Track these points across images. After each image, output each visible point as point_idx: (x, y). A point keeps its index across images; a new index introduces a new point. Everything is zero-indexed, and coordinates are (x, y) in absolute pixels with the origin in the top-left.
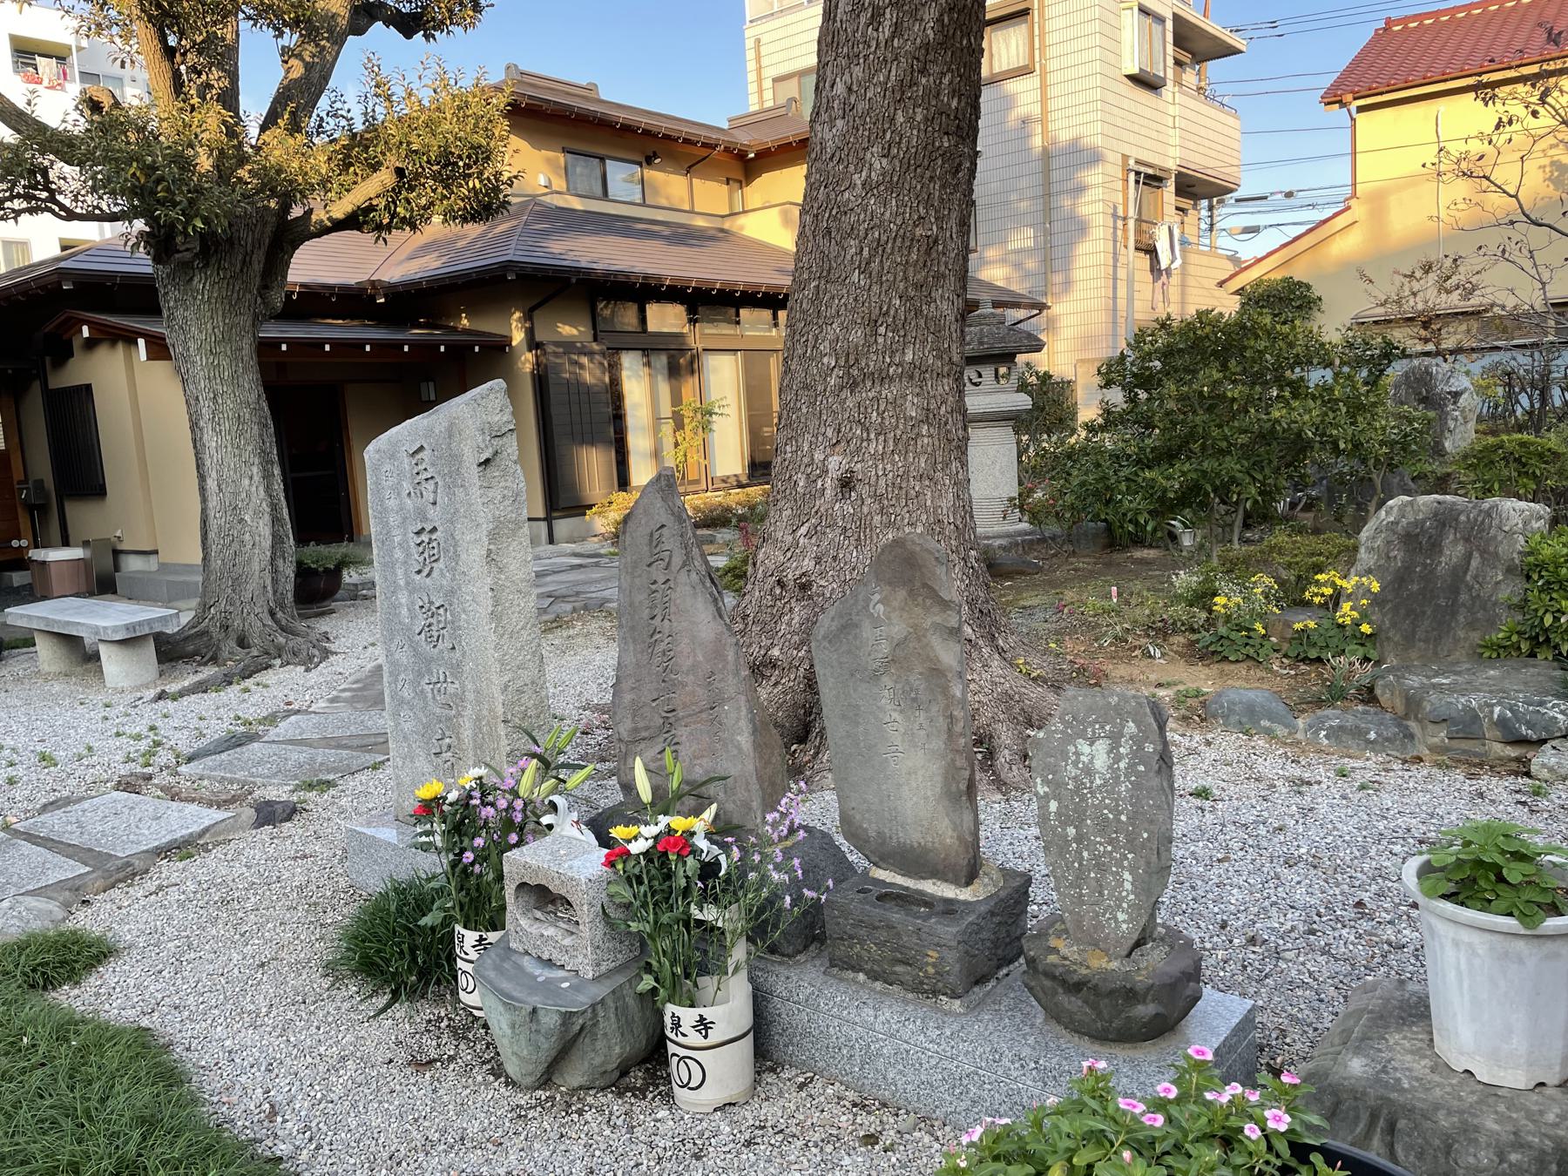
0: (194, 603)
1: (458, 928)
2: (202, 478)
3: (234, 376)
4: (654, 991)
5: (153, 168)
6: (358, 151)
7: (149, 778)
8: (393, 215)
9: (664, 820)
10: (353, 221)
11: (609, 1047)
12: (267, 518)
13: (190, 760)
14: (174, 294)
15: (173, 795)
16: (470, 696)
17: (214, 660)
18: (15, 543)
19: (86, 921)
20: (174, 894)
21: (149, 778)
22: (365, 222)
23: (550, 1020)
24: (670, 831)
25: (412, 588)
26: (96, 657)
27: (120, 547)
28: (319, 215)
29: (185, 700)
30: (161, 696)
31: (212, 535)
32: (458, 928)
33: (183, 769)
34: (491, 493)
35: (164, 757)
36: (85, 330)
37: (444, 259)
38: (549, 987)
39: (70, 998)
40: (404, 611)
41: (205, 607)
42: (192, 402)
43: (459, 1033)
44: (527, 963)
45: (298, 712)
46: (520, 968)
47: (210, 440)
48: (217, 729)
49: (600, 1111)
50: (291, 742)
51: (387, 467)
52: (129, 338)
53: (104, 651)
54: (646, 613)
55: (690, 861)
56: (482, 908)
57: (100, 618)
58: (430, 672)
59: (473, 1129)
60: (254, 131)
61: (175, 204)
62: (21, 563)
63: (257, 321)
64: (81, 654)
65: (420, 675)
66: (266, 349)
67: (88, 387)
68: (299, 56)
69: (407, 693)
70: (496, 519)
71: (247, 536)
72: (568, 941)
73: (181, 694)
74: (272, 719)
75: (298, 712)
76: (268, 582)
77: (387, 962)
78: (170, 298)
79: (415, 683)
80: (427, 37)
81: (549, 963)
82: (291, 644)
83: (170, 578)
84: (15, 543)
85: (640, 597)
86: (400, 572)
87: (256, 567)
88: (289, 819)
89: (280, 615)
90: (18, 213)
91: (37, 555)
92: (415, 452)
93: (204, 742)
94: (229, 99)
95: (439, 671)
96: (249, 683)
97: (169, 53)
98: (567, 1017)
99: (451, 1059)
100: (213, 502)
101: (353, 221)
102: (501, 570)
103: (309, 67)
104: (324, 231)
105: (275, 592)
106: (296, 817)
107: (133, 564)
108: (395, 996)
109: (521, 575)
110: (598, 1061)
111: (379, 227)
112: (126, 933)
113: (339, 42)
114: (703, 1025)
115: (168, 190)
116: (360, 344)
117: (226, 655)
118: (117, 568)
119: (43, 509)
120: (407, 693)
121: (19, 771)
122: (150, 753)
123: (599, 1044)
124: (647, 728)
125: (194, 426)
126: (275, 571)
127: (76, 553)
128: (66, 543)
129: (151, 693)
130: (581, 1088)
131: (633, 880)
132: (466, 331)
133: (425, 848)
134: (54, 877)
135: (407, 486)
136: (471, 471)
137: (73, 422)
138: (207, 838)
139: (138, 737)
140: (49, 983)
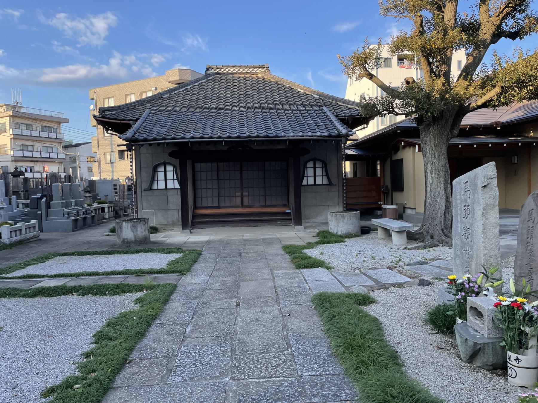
0: (420, 225)
1: (457, 318)
2: (426, 187)
3: (439, 156)
4: (504, 347)
5: (419, 100)
6: (487, 82)
7: (396, 267)
8: (500, 101)
9: (515, 298)
10: (485, 105)
11: (488, 357)
12: (444, 200)
13: (407, 265)
14: (424, 133)
15: (401, 273)
16: (475, 256)
17: (423, 241)
18: (379, 203)
19: (371, 294)
20: (393, 294)
21: (396, 267)
22: (489, 105)
23: (470, 343)
24: (516, 301)
25: (462, 222)
26: (390, 236)
27: (407, 206)
28: (473, 105)
29: (411, 251)
30: (405, 248)
31: (427, 204)
32: (457, 318)
33: (405, 267)
34: (485, 196)
35: (401, 263)
36: (403, 143)
37: (525, 112)
38: (474, 336)
39: (364, 308)
40: (459, 229)
41: (423, 225)
42: (426, 164)
43: (452, 345)
44: (470, 329)
45: (441, 259)
46: (467, 330)
47: (430, 176)
48: (417, 259)
49: (484, 374)
50: (436, 267)
51: (458, 187)
52: (414, 145)
53: (394, 234)
54: (526, 236)
55: (521, 311)
56: (463, 314)
57: (394, 224)
58: (465, 247)
59: (446, 364)
60: (455, 79)
61: (424, 109)
62: (380, 208)
63: (448, 139)
64: (387, 232)
65: (462, 248)
66: (451, 149)
67: (402, 159)
68: (472, 55)
69: (458, 253)
70: (486, 204)
71: (437, 206)
72: (482, 326)
73: (411, 249)
74: (433, 260)
75: (441, 259)
76: (442, 220)
77: (438, 322)
78: (423, 134)
79: (461, 250)
80: (521, 38)
81: (476, 331)
82: (446, 240)
83: (418, 217)
84: (379, 203)
85: (525, 231)
86: (459, 217)
87: (439, 215)
88: (428, 285)
89: (445, 231)
90: (385, 114)
91: (384, 206)
92: (466, 183)
93: (413, 262)
94: (447, 75)
95: (467, 248)
96: (431, 249)
97: (429, 64)
98: (475, 344)
99: (448, 350)
100: (428, 194)
101: (485, 105)
102: (487, 219)
103: (475, 58)
104: (474, 109)
105: (444, 224)
106: (430, 285)
107: (409, 212)
108: (438, 333)
109: (494, 221)
110: (485, 360)
111: (494, 106)
112: (379, 299)
113: (486, 47)
114: (517, 360)
115: (422, 105)
116: (487, 144)
117: (426, 240)
118: (404, 212)
119: (387, 194)
120: (458, 253)
121: (367, 259)
122: (398, 262)
123: (486, 356)
124: (524, 273)
125: (426, 172)
126: (445, 217)
127: (394, 207)
128: (392, 204)
129: (403, 247)
130: (480, 367)
131: (503, 312)
132: (532, 138)
133: (450, 293)
134: (367, 284)
135: (463, 192)
136: (480, 189)
137: (397, 168)
138: (405, 285)
139: (396, 257)
140: (360, 304)
